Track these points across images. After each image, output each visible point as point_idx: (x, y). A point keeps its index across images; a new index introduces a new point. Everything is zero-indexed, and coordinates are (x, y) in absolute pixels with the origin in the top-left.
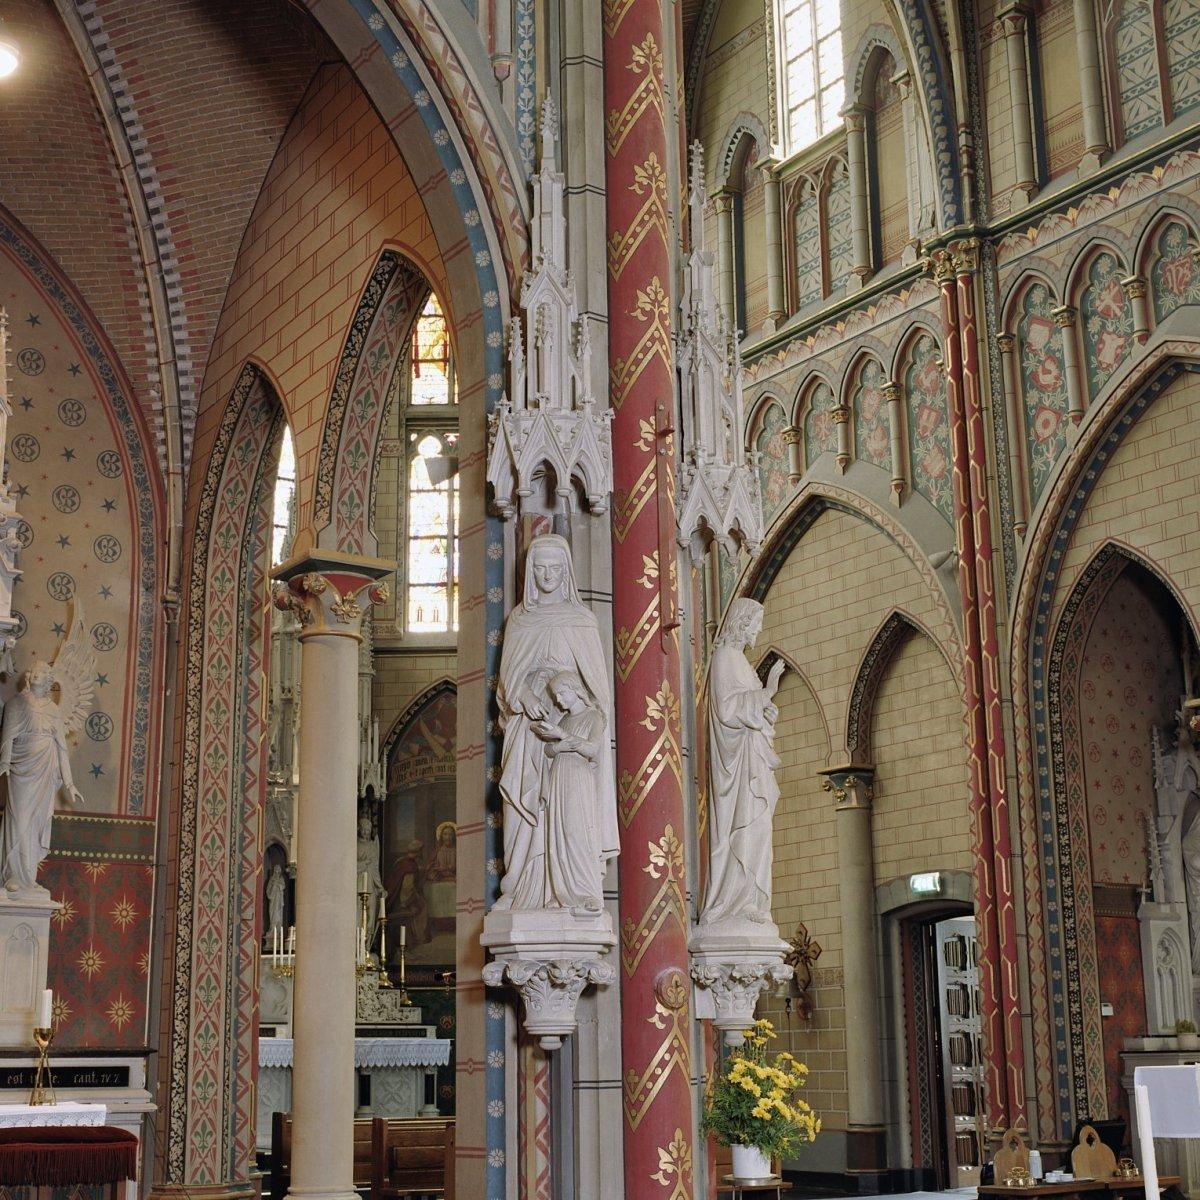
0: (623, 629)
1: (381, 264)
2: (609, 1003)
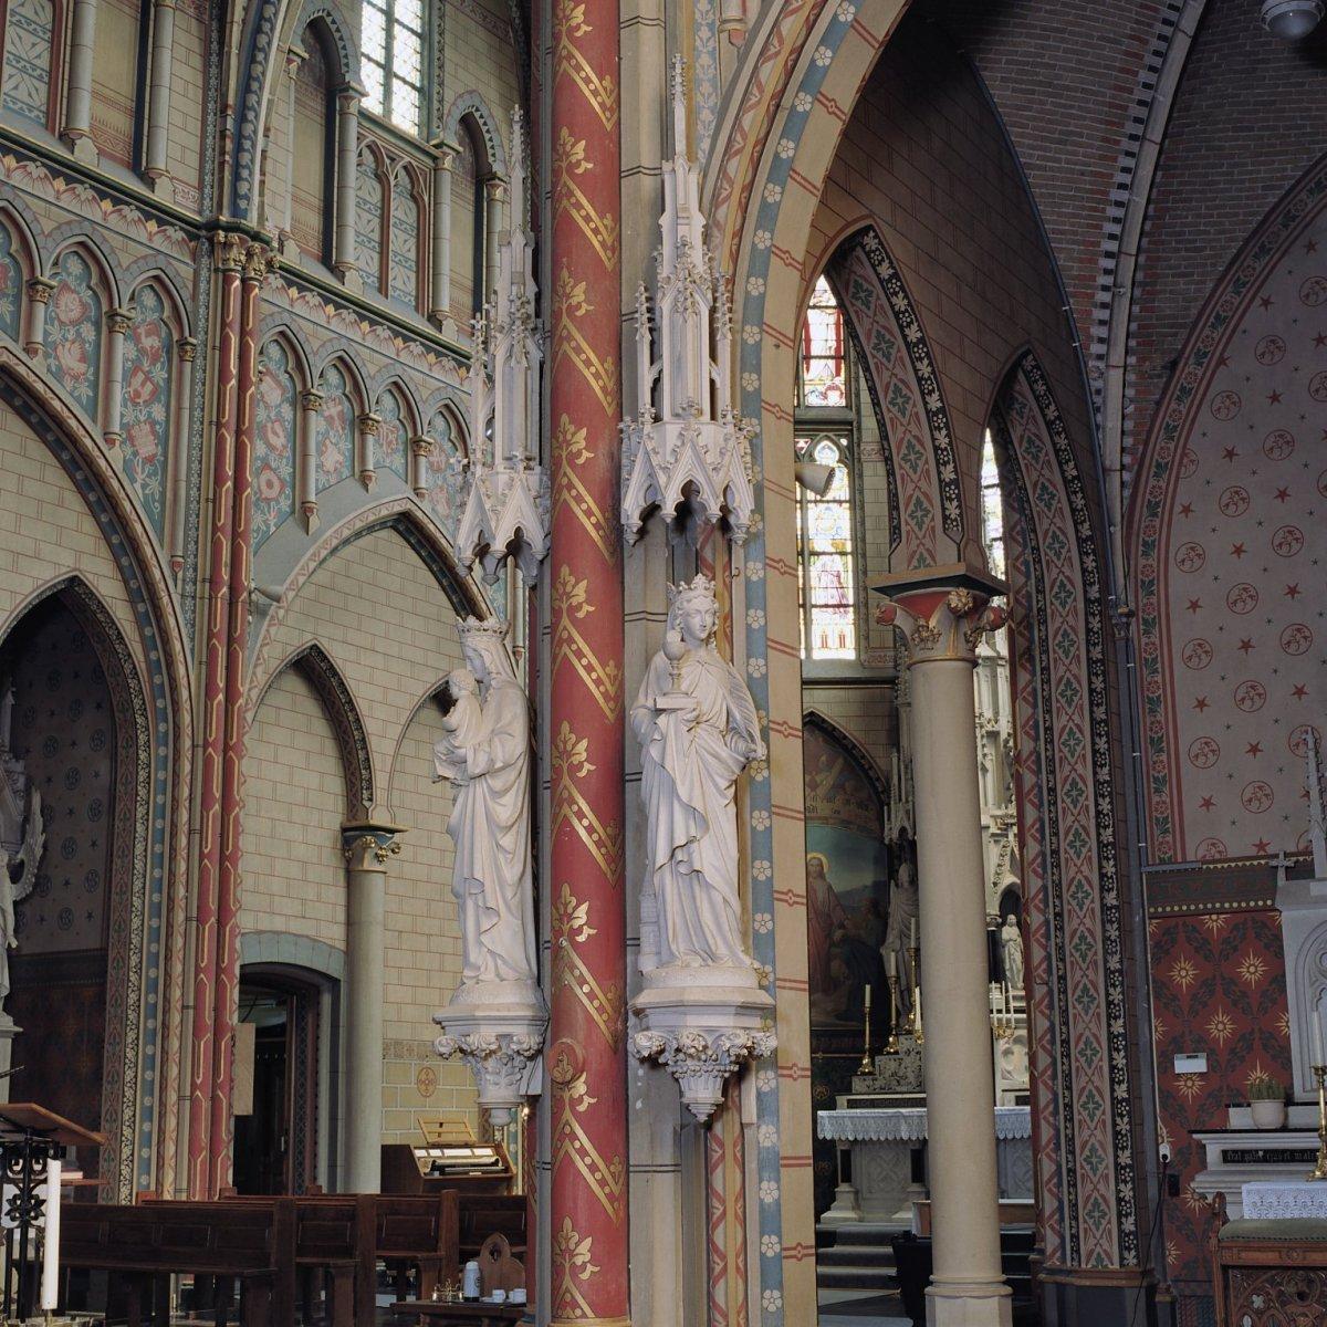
1: (1171, 853)
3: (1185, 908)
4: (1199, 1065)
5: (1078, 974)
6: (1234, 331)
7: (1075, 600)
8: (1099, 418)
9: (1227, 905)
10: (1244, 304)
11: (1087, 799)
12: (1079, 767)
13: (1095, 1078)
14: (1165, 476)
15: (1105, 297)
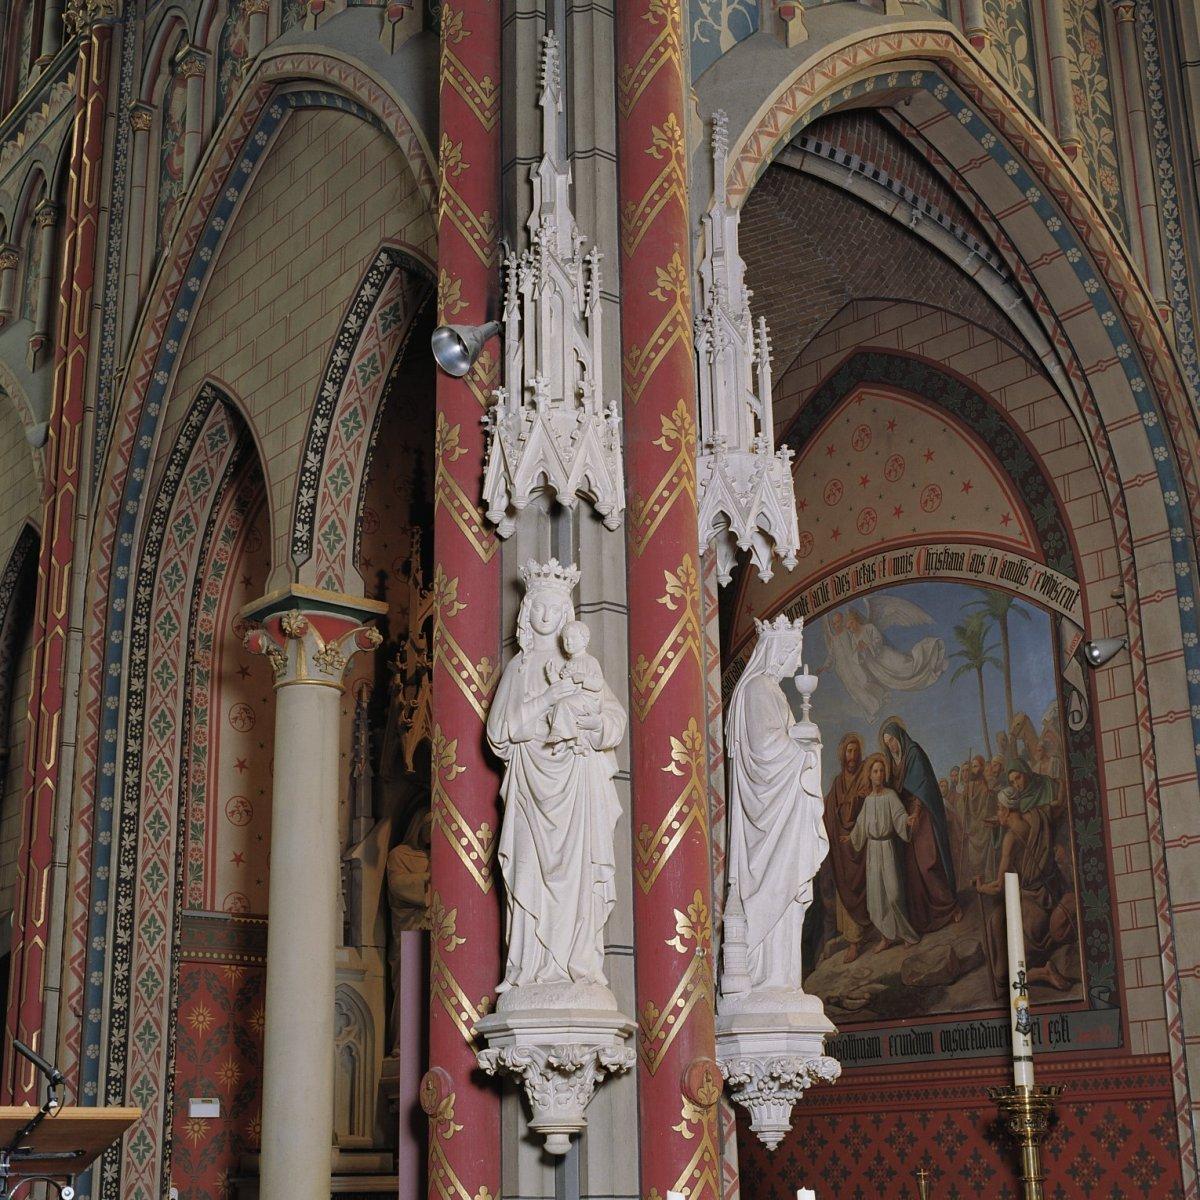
0: (646, 827)
2: (626, 1090)
3: (208, 955)
5: (142, 1010)
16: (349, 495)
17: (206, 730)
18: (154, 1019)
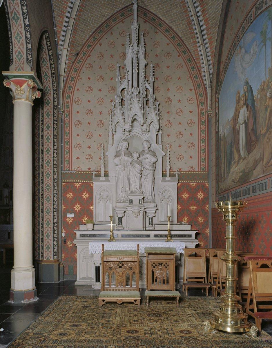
4: (73, 216)
5: (47, 194)
6: (92, 50)
7: (51, 105)
8: (60, 61)
9: (81, 181)
10: (95, 44)
11: (51, 153)
12: (50, 145)
13: (49, 218)
14: (73, 81)
15: (65, 29)
16: (23, 42)
17: (69, 128)
18: (50, 196)
